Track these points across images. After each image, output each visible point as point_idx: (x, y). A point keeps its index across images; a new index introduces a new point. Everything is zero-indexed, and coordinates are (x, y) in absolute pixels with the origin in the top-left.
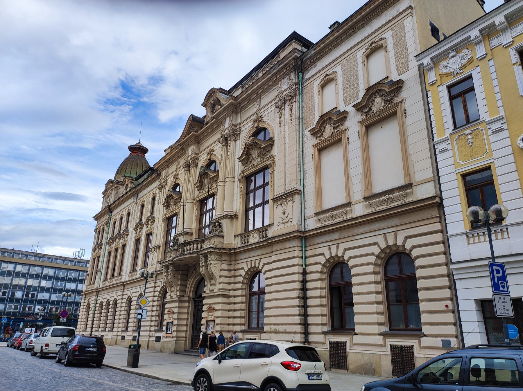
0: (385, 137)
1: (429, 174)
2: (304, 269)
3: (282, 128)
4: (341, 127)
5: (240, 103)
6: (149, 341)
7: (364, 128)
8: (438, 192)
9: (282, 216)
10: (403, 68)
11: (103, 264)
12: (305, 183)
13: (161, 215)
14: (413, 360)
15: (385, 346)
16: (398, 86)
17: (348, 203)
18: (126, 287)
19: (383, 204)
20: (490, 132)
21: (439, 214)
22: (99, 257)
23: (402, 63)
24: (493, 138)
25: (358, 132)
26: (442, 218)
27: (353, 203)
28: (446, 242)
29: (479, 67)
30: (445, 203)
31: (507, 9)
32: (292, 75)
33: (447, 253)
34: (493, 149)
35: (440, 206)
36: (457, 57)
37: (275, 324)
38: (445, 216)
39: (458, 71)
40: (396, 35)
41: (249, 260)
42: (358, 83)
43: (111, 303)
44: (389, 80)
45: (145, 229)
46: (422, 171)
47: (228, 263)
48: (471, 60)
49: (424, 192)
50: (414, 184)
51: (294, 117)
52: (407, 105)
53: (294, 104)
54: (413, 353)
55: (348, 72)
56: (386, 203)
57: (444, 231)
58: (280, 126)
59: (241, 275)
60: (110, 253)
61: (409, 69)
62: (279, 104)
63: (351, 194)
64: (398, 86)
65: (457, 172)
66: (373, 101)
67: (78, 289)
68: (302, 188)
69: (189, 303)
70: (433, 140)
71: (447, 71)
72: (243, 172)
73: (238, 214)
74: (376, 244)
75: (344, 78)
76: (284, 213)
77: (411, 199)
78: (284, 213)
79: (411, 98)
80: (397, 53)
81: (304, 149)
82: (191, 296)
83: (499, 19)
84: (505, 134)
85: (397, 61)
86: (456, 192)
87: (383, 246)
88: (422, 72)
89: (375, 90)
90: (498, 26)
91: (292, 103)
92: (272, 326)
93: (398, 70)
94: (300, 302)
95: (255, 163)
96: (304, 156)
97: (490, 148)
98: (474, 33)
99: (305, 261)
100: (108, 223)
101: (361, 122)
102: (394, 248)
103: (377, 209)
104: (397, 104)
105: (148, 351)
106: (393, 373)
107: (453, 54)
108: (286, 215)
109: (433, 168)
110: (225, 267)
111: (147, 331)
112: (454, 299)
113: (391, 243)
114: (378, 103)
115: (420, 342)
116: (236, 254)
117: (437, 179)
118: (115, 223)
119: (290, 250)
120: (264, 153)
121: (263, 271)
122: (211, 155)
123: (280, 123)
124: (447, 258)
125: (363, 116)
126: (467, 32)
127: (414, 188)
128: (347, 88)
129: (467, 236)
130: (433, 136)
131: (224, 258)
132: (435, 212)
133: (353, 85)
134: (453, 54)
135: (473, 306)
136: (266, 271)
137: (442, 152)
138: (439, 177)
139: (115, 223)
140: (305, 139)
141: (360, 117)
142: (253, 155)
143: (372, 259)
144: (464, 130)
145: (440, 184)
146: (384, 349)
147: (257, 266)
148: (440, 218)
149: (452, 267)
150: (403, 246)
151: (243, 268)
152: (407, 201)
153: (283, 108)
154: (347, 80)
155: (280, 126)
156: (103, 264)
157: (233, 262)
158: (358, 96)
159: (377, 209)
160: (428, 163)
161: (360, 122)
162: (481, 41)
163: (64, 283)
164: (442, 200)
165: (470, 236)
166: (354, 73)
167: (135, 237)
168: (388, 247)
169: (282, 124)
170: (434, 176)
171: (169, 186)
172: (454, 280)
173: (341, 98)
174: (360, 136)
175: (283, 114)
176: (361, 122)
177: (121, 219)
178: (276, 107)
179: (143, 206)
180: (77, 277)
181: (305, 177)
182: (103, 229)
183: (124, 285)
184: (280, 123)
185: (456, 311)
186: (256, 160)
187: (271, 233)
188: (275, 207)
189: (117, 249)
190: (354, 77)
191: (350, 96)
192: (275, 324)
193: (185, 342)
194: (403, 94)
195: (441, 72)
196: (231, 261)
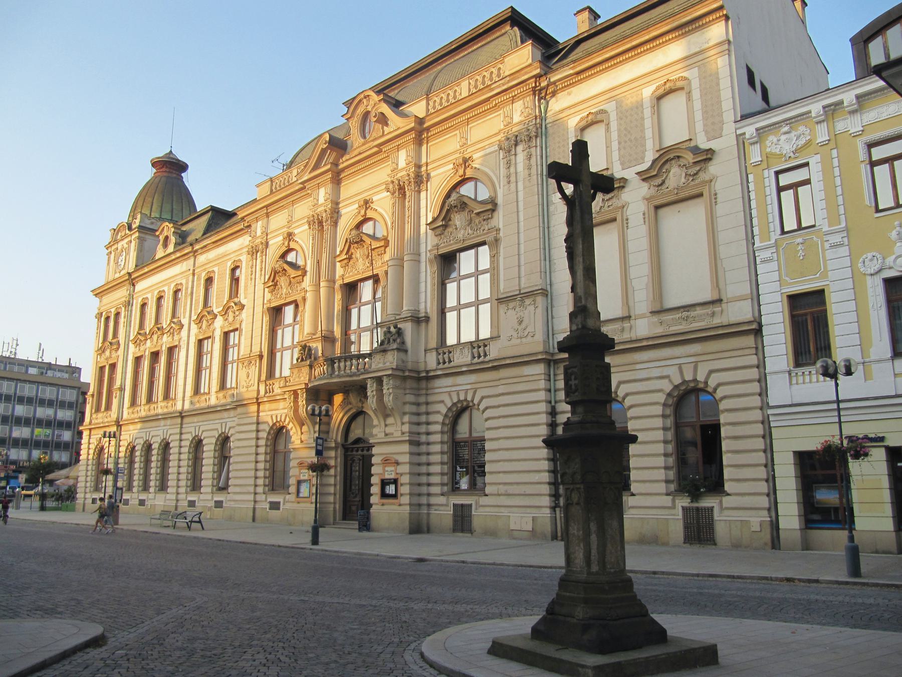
0: (685, 226)
1: (746, 289)
2: (553, 408)
3: (513, 185)
4: (614, 200)
5: (428, 129)
6: (254, 509)
7: (652, 209)
8: (757, 314)
9: (516, 326)
10: (715, 132)
11: (124, 376)
12: (553, 279)
13: (259, 302)
14: (712, 524)
15: (673, 507)
16: (706, 156)
17: (626, 317)
18: (186, 420)
19: (680, 324)
20: (827, 245)
21: (756, 344)
22: (113, 366)
23: (713, 123)
24: (829, 254)
25: (644, 214)
26: (759, 350)
27: (633, 317)
28: (762, 380)
29: (819, 156)
30: (765, 331)
31: (860, 87)
32: (529, 99)
33: (763, 393)
34: (829, 268)
35: (758, 332)
36: (793, 134)
37: (505, 484)
38: (763, 347)
39: (792, 155)
40: (704, 78)
41: (454, 389)
42: (643, 138)
43: (138, 448)
44: (692, 144)
45: (219, 322)
46: (737, 284)
47: (416, 392)
48: (808, 144)
49: (738, 312)
50: (725, 300)
51: (534, 171)
52: (718, 186)
53: (533, 150)
54: (712, 516)
55: (627, 117)
56: (684, 323)
57: (761, 365)
58: (509, 182)
59: (438, 412)
60: (138, 360)
61: (723, 134)
62: (506, 145)
63: (631, 304)
64: (706, 156)
65: (783, 291)
66: (668, 171)
67: (58, 418)
68: (549, 287)
69: (336, 451)
70: (754, 244)
71: (777, 151)
72: (437, 246)
73: (430, 315)
74: (668, 377)
75: (620, 124)
76: (520, 322)
77: (719, 321)
78: (520, 322)
79: (723, 173)
80: (706, 106)
81: (552, 224)
82: (339, 439)
83: (848, 97)
84: (844, 251)
85: (705, 119)
86: (779, 318)
87: (677, 380)
88: (741, 142)
89: (672, 156)
90: (847, 107)
91: (530, 147)
92: (501, 486)
93: (706, 132)
94: (548, 453)
95: (460, 235)
96: (551, 236)
97: (825, 267)
98: (816, 108)
99: (555, 395)
100: (128, 304)
101: (648, 199)
102: (692, 385)
103: (671, 329)
104: (704, 183)
105: (254, 524)
106: (685, 539)
107: (786, 129)
108: (523, 325)
109: (750, 281)
110: (410, 398)
111: (249, 493)
112: (769, 450)
113: (688, 377)
114: (675, 176)
115: (721, 502)
116: (429, 378)
117: (756, 297)
118: (144, 305)
119: (531, 378)
120: (477, 221)
121: (482, 407)
122: (367, 209)
123: (509, 177)
124: (762, 401)
125: (653, 191)
126: (807, 105)
127: (724, 305)
128: (626, 142)
129: (790, 374)
130: (753, 238)
131: (410, 384)
132: (750, 340)
133: (636, 139)
134: (786, 129)
135: (791, 458)
136: (487, 408)
137: (764, 261)
138: (759, 295)
139: (144, 305)
140: (552, 208)
141: (644, 190)
142: (458, 223)
143: (661, 398)
144: (793, 237)
145: (759, 305)
146: (673, 512)
147: (469, 399)
148: (757, 348)
149: (770, 412)
150: (706, 383)
151: (442, 402)
152: (714, 322)
153: (513, 152)
154: (626, 129)
155: (509, 182)
156: (124, 376)
157: (424, 392)
158: (643, 158)
159: (671, 329)
160: (745, 274)
161: (647, 199)
162: (823, 121)
163: (11, 406)
164: (760, 325)
165: (793, 374)
166: (636, 120)
167: (196, 335)
168: (684, 382)
169: (513, 179)
170: (751, 293)
171: (274, 251)
172: (770, 428)
173: (615, 156)
174: (647, 220)
175: (513, 162)
176: (648, 199)
177: (160, 298)
178: (501, 149)
179: (209, 281)
180: (54, 397)
181: (553, 269)
182: (118, 314)
183: (182, 417)
184: (509, 177)
185: (770, 465)
186: (462, 232)
187: (494, 352)
188: (502, 312)
189: (155, 355)
190: (636, 126)
191: (630, 155)
192: (505, 484)
193: (335, 508)
194: (713, 168)
195: (768, 150)
196: (419, 389)
